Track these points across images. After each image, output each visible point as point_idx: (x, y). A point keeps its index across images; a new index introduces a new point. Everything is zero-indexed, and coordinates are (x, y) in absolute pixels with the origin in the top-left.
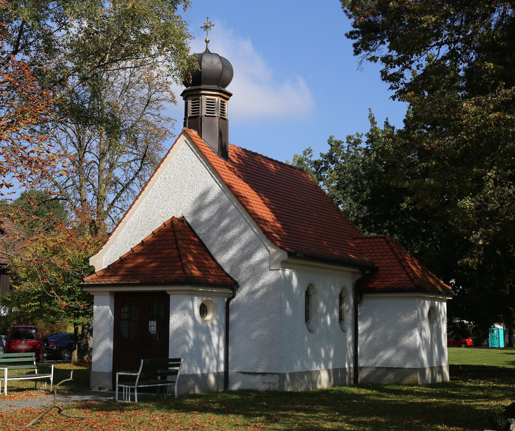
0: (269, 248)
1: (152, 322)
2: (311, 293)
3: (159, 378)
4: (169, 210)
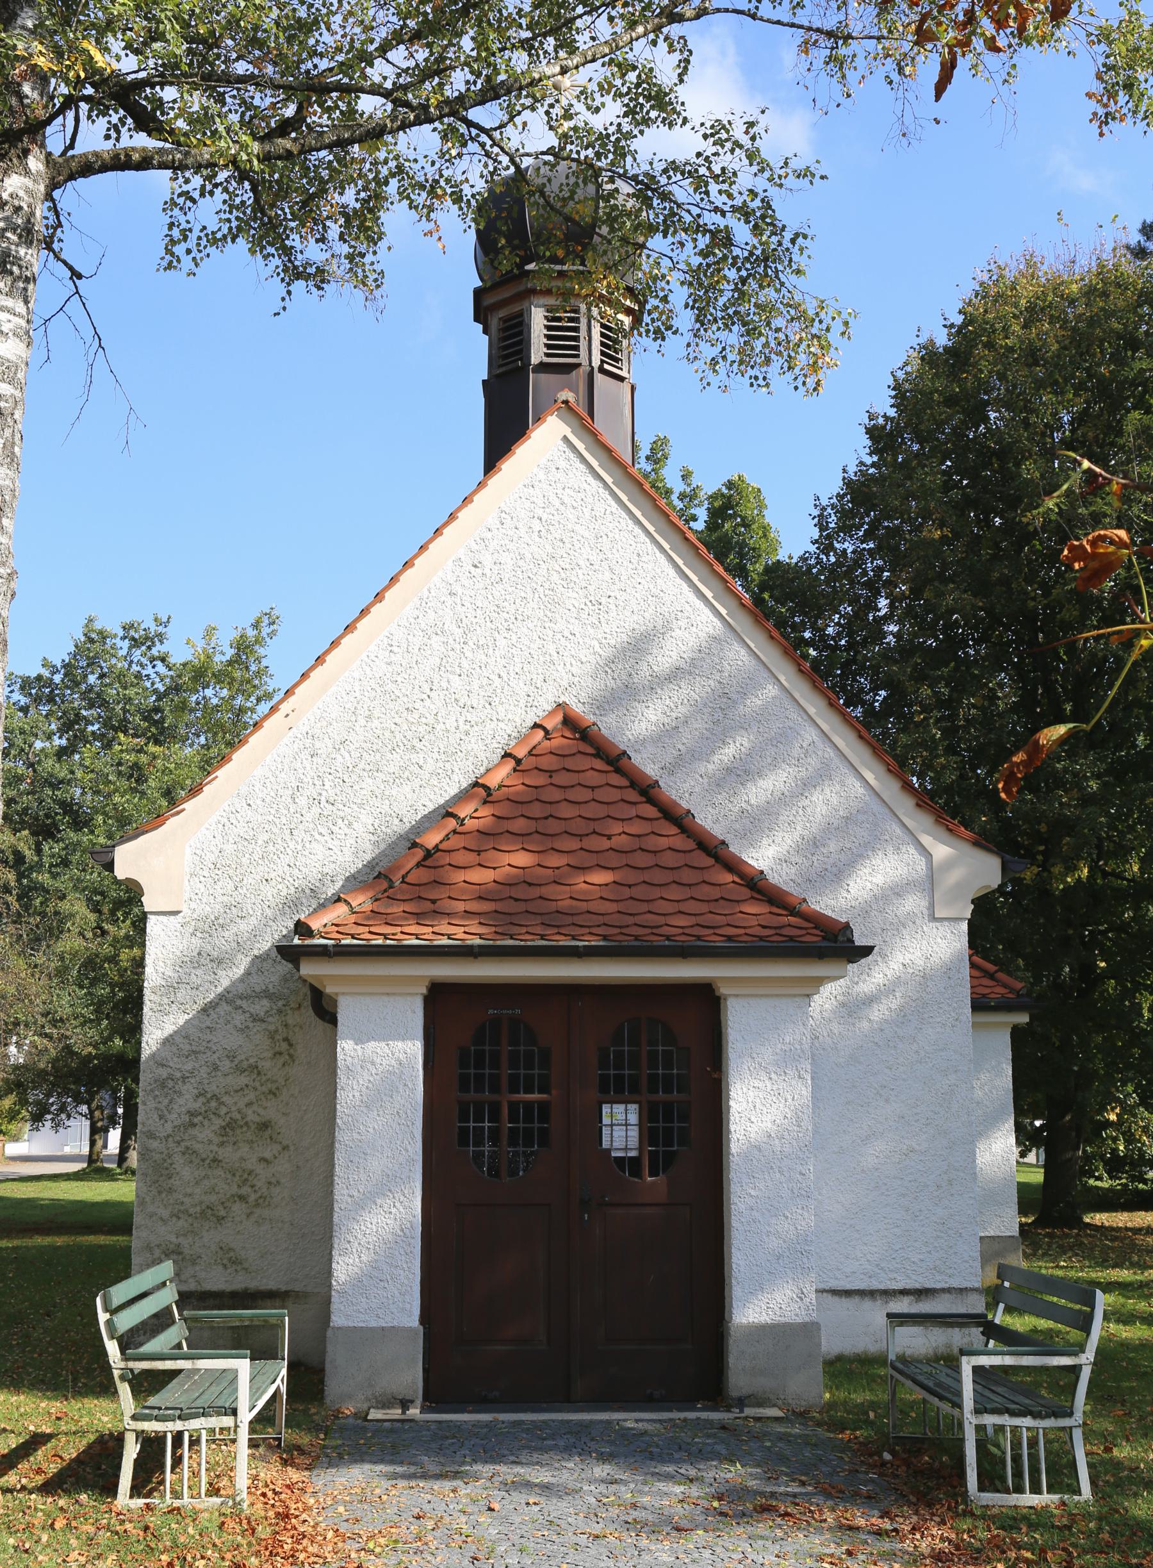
0: (926, 840)
1: (619, 1108)
4: (497, 681)
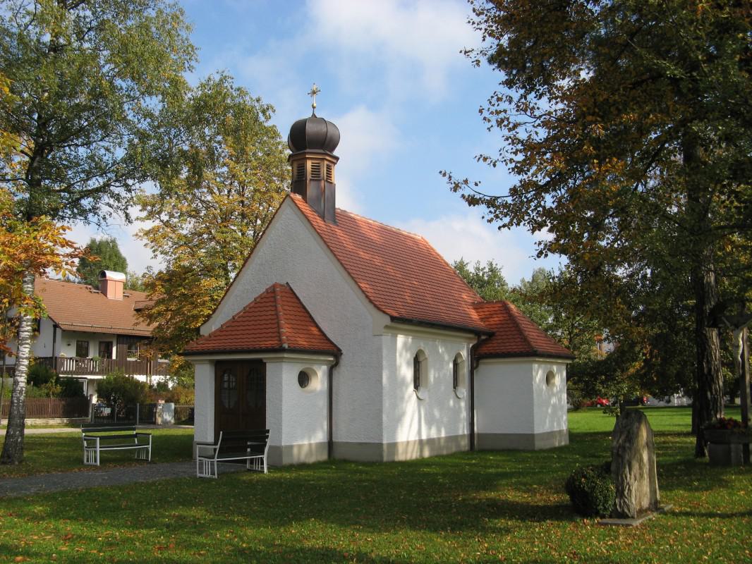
2: (421, 359)
3: (249, 450)
